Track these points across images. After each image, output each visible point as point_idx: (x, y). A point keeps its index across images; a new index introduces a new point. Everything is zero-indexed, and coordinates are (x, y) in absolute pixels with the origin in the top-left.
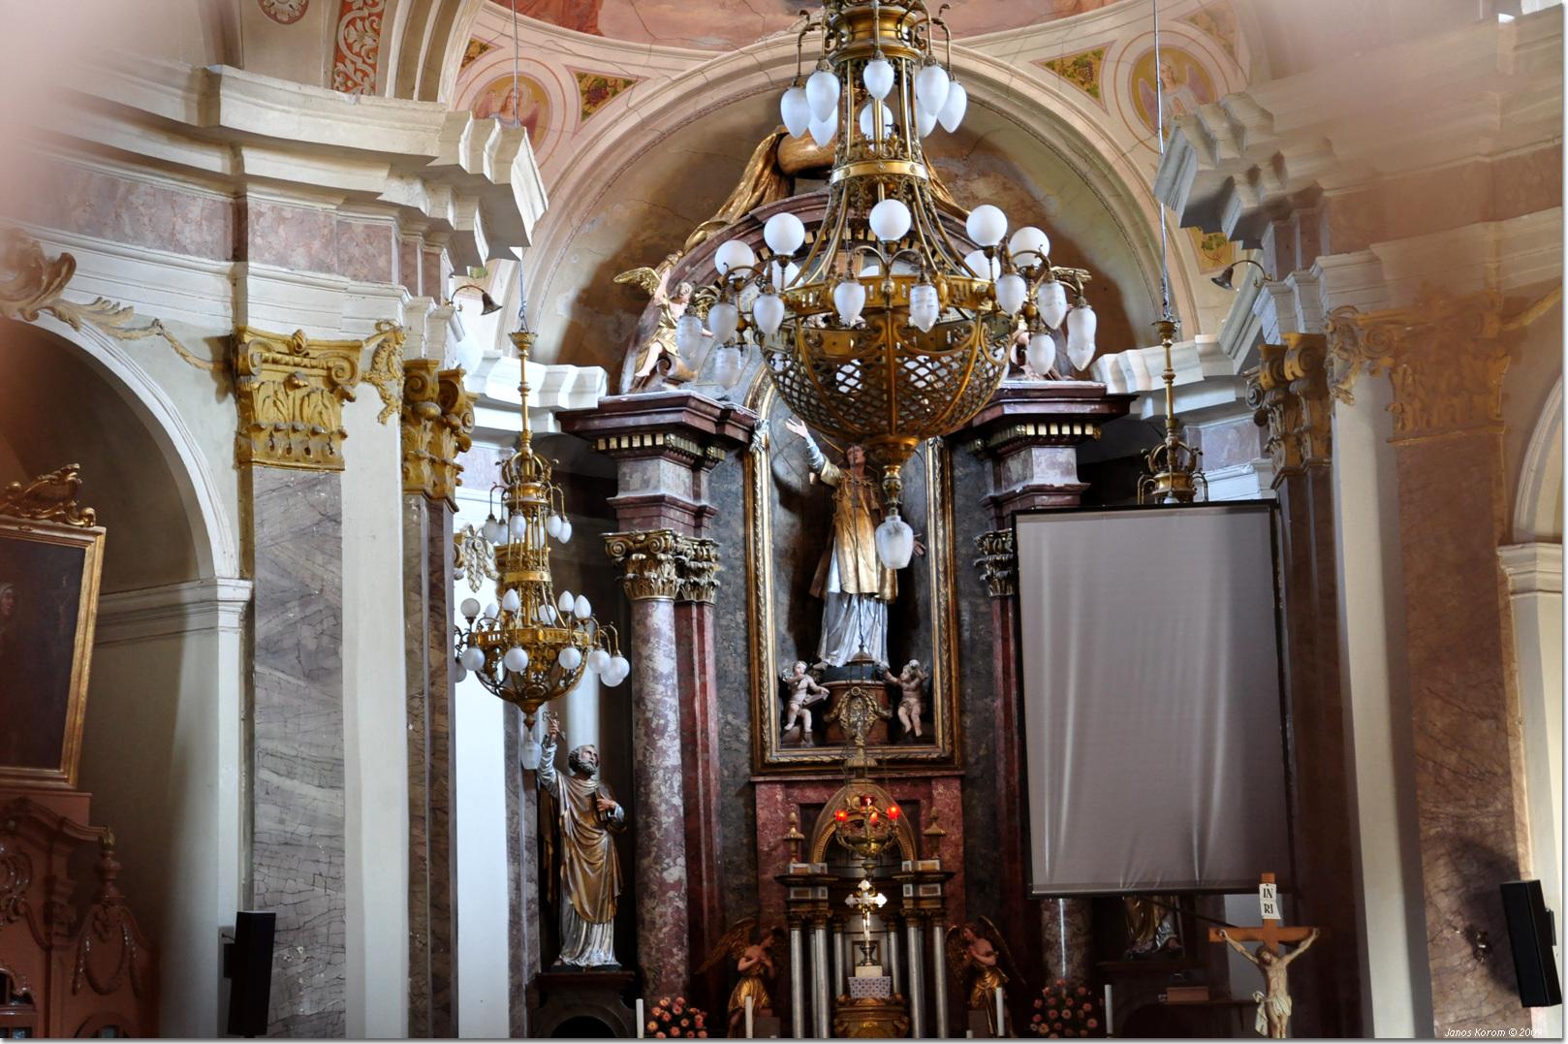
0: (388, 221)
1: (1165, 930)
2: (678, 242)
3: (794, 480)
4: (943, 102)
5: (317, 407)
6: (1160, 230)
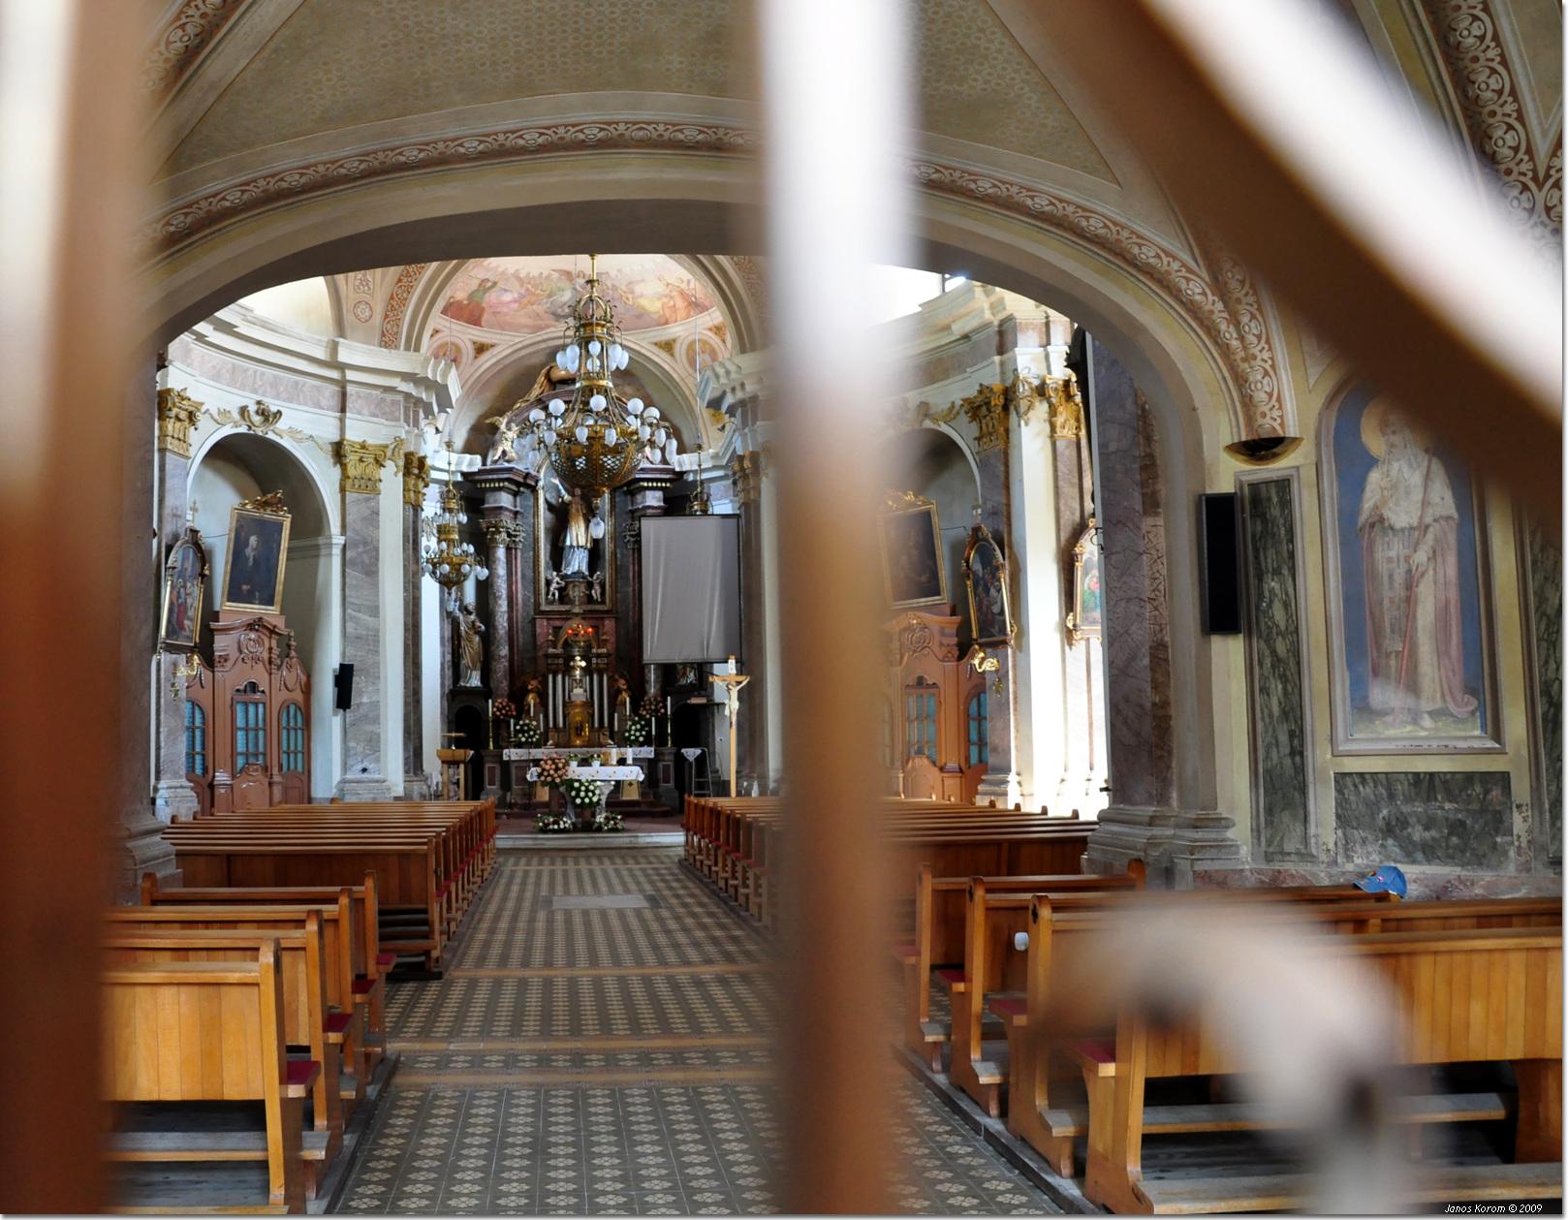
0: (400, 398)
1: (691, 677)
2: (510, 407)
3: (553, 501)
4: (620, 358)
5: (371, 469)
6: (697, 410)
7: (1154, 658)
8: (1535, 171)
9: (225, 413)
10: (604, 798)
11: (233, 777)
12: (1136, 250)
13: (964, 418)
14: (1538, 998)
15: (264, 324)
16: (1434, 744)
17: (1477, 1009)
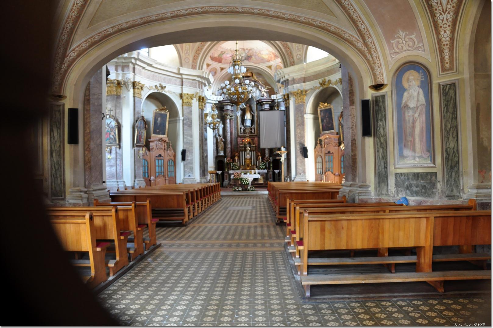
5: (190, 100)
7: (352, 143)
8: (443, 9)
9: (151, 87)
10: (250, 183)
11: (156, 178)
12: (343, 35)
13: (339, 84)
14: (418, 231)
15: (160, 64)
16: (419, 165)
17: (401, 233)
